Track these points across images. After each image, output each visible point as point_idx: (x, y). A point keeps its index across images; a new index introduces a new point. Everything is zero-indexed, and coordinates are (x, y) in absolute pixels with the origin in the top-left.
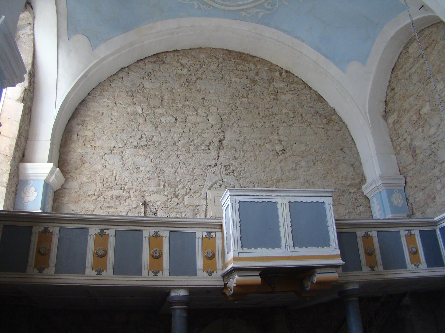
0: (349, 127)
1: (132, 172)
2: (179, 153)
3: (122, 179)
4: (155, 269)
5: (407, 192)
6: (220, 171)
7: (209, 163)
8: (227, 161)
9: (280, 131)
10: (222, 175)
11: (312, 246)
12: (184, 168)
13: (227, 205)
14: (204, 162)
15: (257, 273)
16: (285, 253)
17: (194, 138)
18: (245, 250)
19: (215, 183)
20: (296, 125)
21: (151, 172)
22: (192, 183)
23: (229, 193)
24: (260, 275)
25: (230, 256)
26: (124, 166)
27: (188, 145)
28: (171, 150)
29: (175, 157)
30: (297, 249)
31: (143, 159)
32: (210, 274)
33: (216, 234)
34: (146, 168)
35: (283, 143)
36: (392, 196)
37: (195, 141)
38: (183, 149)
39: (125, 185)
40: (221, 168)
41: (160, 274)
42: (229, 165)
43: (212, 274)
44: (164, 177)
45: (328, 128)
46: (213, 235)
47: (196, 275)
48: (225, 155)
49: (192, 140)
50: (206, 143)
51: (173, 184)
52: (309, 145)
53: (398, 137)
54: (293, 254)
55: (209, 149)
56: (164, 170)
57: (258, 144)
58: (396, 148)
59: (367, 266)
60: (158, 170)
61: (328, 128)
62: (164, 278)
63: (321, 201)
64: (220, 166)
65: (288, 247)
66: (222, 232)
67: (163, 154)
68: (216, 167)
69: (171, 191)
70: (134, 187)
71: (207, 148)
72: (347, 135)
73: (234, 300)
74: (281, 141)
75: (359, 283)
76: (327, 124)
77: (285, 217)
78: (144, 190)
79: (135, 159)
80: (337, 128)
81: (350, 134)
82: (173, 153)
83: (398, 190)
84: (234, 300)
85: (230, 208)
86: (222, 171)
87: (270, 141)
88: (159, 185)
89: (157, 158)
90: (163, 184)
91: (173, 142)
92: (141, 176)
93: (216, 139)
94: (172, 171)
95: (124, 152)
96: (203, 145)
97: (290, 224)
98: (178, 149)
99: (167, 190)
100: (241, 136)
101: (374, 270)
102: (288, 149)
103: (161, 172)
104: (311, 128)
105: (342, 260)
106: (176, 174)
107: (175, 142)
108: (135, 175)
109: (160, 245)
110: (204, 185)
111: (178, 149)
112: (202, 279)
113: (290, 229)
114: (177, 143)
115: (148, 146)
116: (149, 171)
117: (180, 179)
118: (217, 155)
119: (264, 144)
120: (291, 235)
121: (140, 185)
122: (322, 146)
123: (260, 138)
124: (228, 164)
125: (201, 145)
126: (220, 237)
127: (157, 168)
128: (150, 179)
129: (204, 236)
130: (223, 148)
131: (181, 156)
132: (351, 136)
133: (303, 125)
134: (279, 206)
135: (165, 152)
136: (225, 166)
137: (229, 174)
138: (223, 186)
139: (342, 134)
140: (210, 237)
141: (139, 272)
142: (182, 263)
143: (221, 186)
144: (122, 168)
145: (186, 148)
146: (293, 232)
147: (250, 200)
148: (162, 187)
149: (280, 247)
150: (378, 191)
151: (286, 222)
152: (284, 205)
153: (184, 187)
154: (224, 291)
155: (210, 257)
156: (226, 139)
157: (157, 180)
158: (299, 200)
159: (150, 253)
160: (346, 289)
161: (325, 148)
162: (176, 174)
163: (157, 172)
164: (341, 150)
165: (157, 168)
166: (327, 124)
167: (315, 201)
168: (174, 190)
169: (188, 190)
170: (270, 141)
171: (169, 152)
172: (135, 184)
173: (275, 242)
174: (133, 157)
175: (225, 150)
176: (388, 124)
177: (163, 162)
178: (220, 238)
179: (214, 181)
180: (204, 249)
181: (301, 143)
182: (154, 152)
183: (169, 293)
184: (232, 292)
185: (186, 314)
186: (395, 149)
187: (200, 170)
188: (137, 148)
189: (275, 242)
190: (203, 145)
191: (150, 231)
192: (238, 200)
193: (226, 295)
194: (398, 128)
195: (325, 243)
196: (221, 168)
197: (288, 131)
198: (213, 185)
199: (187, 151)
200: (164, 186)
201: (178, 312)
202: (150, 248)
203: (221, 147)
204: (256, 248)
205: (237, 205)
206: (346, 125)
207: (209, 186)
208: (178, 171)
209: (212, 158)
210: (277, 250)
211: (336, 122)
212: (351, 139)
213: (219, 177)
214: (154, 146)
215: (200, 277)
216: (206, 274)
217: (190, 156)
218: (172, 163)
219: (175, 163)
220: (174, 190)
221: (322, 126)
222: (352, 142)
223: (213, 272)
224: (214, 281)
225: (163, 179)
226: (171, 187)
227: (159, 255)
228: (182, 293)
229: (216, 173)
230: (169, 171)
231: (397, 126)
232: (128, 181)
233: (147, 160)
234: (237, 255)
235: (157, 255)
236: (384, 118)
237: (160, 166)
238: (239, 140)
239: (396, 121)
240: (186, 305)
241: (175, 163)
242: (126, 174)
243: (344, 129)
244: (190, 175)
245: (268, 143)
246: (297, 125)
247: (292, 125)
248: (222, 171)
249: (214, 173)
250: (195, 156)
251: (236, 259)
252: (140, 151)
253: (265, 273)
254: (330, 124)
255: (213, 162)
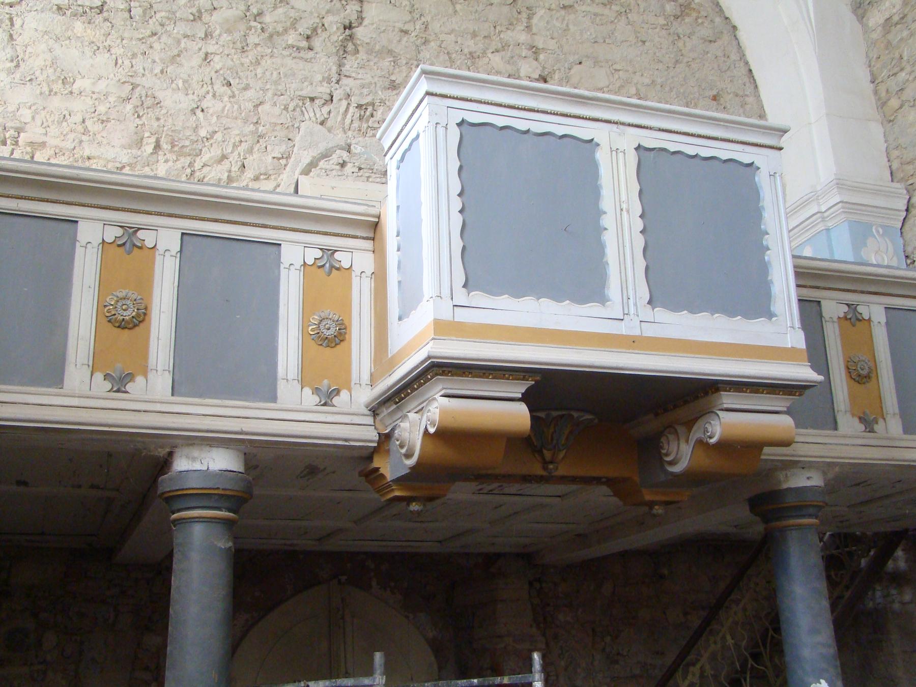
0: (742, 35)
1: (46, 89)
2: (211, 49)
3: (10, 109)
4: (119, 365)
5: (908, 235)
6: (344, 119)
7: (307, 91)
8: (365, 91)
9: (535, 21)
10: (350, 133)
11: (713, 311)
12: (226, 99)
13: (413, 135)
14: (294, 86)
15: (518, 389)
16: (619, 325)
17: (264, 7)
18: (479, 298)
19: (326, 155)
20: (584, 8)
21: (112, 99)
22: (252, 148)
23: (424, 86)
24: (525, 398)
25: (423, 316)
26: (18, 66)
27: (242, 27)
28: (186, 36)
29: (197, 60)
30: (661, 314)
31: (88, 52)
32: (328, 397)
33: (356, 257)
34: (94, 84)
35: (542, 57)
36: (865, 245)
37: (267, 19)
38: (226, 37)
39: (19, 131)
40: (347, 108)
41: (136, 387)
42: (373, 104)
43: (336, 400)
44: (158, 119)
45: (680, 31)
46: (343, 259)
47: (274, 399)
48: (361, 71)
49: (255, 11)
50: (304, 28)
51: (187, 143)
52: (621, 73)
53: (896, 70)
54: (650, 331)
55: (310, 49)
56: (160, 95)
57: (466, 51)
58: (884, 104)
59: (853, 415)
60: (137, 95)
61: (681, 28)
62: (152, 403)
63: (746, 160)
64: (344, 103)
65: (631, 302)
66: (379, 253)
67: (157, 46)
68: (331, 107)
69: (179, 165)
70: (52, 141)
71: (304, 44)
72: (734, 56)
73: (409, 500)
74: (535, 51)
75: (825, 467)
76: (676, 17)
77: (624, 198)
78: (87, 153)
79: (58, 51)
80: (705, 31)
81: (743, 57)
82: (194, 46)
83: (882, 226)
84: (409, 500)
85: (425, 146)
86: (348, 121)
87: (505, 46)
88: (139, 143)
89: (134, 55)
90: (153, 140)
91: (194, 10)
92: (79, 106)
93: (336, 18)
94: (187, 102)
95: (18, 22)
96: (291, 32)
97: (639, 225)
98: (208, 35)
99: (166, 161)
100: (413, 21)
101: (872, 431)
102: (556, 76)
103: (149, 102)
104: (629, 23)
105: (812, 367)
106: (198, 112)
107: (199, 11)
108: (56, 103)
109: (144, 281)
110: (288, 158)
111: (208, 35)
112: (295, 413)
113: (640, 242)
114: (206, 17)
115: (105, 14)
116: (106, 95)
117: (211, 129)
118: (334, 69)
119: (484, 53)
120: (641, 264)
121: (71, 136)
122: (659, 80)
123: (474, 35)
124: (369, 99)
125: (286, 30)
126: (370, 267)
127: (134, 87)
128: (108, 121)
129: (310, 261)
130: (357, 52)
131: (217, 58)
132: (747, 63)
133: (606, 11)
134: (602, 156)
135: (164, 38)
136: (359, 106)
137: (370, 133)
138: (349, 165)
139: (720, 54)
140: (332, 267)
141: (53, 374)
142: (226, 350)
143: (343, 165)
144: (10, 72)
145: (237, 35)
146: (648, 253)
147: (500, 122)
148: (149, 149)
149: (602, 299)
150: (821, 227)
151: (625, 213)
152: (621, 155)
153: (224, 157)
154: (376, 463)
155: (331, 337)
156: (365, 22)
157: (132, 127)
158: (672, 144)
159: (102, 305)
160: (785, 486)
161: (667, 89)
162: (198, 112)
163: (135, 101)
164: (715, 98)
165: (134, 87)
166: (676, 17)
167: (724, 155)
168: (191, 165)
169: (235, 168)
170: (505, 46)
171: (179, 42)
172: (54, 130)
173: (587, 285)
174: (51, 42)
175: (362, 55)
176: (866, 30)
177: (157, 70)
178: (369, 273)
179: (322, 147)
180: (308, 305)
181: (596, 62)
182: (126, 35)
183: (164, 464)
184: (411, 462)
185: (230, 544)
186: (882, 104)
187: (277, 110)
188: (68, 13)
189: (587, 285)
190: (291, 32)
191: (106, 223)
192: (458, 116)
193: (383, 476)
194: (902, 39)
195: (757, 305)
196: (347, 108)
197: (558, 24)
198: (319, 160)
199: (239, 45)
200: (158, 146)
201: (198, 530)
202: (104, 284)
203: (350, 47)
204: (518, 293)
205: (454, 134)
206: (735, 28)
207: (306, 160)
208: (204, 105)
209: (319, 77)
210: (592, 309)
211: (703, 13)
212: (744, 71)
213: (340, 138)
214: (127, 15)
215: (289, 406)
216: (310, 399)
217: (246, 61)
218: (185, 77)
219: (195, 78)
220: (191, 165)
221: (662, 21)
222: (746, 79)
223: (337, 392)
224: (346, 422)
225: (155, 124)
226: (181, 154)
227: (138, 315)
228: (221, 461)
229: (329, 123)
230: (175, 101)
231: (896, 35)
232: (29, 119)
233: (103, 58)
234: (446, 314)
235: (128, 314)
236: (854, 11)
237: (147, 82)
238: (406, 32)
239: (896, 18)
240: (229, 510)
241: (195, 78)
242: (26, 94)
243: (726, 38)
244: (246, 121)
245: (497, 51)
246: (588, 9)
247: (571, 6)
248: (348, 121)
249: (322, 123)
250: (263, 62)
251: (442, 328)
252: (79, 26)
253: (549, 390)
254: (687, 20)
255: (320, 89)
